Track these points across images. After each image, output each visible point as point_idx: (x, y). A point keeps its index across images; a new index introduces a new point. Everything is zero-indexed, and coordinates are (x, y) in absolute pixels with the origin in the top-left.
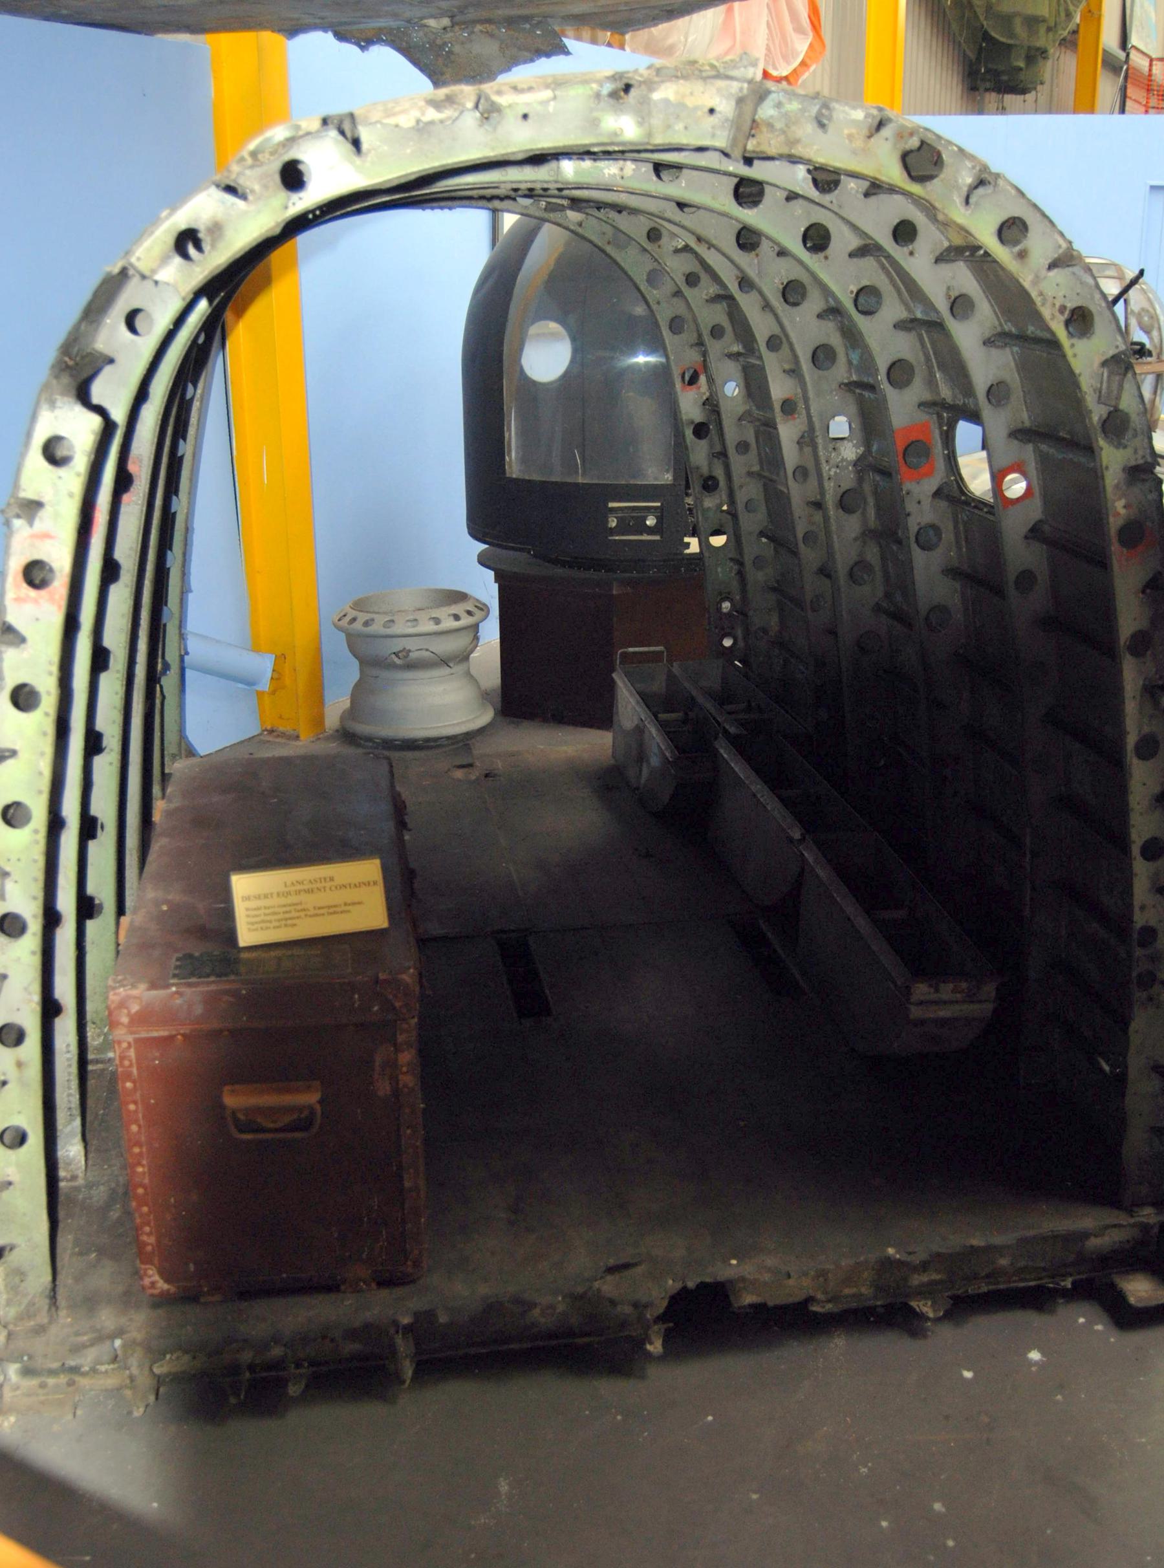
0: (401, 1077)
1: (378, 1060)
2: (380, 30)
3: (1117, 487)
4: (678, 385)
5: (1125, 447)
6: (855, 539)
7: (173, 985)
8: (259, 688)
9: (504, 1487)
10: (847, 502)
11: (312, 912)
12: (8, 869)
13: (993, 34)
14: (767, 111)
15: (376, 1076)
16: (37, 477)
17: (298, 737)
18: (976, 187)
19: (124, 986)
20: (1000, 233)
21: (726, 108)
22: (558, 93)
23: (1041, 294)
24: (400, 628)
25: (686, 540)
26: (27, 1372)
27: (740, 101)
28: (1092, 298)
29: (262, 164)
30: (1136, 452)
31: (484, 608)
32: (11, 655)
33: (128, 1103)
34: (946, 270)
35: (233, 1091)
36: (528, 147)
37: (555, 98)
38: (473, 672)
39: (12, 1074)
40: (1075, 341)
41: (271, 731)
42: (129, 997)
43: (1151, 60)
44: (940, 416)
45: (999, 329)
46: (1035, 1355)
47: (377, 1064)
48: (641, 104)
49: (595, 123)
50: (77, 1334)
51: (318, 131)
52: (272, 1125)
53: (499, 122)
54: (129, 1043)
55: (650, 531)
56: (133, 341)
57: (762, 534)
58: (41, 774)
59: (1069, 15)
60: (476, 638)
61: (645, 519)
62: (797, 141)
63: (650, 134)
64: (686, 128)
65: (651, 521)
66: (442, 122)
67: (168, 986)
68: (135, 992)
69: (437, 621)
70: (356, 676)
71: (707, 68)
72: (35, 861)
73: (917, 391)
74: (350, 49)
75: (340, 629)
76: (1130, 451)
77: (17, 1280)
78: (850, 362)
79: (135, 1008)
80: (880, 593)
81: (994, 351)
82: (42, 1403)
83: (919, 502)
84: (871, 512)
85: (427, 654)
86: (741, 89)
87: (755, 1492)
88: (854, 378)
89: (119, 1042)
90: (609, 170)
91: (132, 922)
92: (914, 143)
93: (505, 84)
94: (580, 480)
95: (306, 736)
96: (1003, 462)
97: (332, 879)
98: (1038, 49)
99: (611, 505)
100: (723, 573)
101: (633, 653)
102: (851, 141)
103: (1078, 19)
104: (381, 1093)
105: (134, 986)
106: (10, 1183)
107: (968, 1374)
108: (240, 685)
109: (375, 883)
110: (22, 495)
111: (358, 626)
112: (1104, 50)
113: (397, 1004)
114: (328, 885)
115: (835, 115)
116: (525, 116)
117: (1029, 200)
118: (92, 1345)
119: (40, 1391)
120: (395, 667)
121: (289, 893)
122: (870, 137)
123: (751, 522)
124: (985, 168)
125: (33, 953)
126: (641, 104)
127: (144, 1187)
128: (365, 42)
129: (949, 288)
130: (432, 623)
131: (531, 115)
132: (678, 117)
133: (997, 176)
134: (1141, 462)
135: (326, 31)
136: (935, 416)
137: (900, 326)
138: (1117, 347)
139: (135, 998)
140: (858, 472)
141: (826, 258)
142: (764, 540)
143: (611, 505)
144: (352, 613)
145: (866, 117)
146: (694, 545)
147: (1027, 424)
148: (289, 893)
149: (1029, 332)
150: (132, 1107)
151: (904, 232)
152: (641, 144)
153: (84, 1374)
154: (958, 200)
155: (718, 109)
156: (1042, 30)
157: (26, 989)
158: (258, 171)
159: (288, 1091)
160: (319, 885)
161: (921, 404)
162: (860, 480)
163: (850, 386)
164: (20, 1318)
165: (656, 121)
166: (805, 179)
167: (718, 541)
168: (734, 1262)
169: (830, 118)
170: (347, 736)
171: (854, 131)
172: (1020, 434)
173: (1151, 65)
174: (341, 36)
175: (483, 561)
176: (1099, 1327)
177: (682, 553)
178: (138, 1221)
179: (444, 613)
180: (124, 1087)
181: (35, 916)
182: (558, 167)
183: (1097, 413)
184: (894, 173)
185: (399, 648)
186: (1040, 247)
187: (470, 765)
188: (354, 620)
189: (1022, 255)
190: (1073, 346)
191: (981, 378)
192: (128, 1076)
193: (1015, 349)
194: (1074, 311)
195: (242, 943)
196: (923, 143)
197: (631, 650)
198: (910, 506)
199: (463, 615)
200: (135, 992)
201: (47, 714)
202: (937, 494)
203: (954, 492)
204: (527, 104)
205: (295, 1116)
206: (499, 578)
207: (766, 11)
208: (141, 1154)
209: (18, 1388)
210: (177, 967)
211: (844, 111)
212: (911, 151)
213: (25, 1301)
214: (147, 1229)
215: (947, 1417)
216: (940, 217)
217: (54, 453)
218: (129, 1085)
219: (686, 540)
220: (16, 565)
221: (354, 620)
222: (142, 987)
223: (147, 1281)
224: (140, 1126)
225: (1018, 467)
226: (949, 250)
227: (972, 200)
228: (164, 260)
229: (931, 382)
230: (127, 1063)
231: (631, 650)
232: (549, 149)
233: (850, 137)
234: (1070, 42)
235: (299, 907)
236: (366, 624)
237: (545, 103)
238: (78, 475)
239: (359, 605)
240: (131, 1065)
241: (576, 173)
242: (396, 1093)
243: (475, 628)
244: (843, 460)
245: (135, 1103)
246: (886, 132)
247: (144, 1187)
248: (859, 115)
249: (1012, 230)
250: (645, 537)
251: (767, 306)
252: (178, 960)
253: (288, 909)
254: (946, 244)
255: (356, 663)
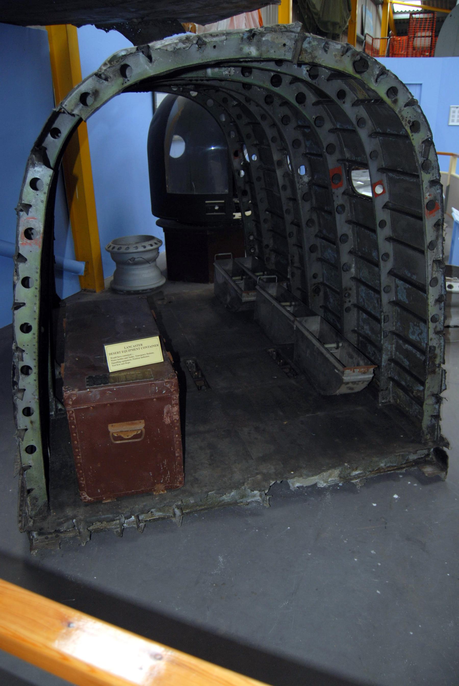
0: (174, 416)
1: (165, 411)
2: (114, 24)
3: (426, 188)
4: (232, 157)
5: (429, 173)
6: (308, 211)
7: (88, 388)
8: (80, 274)
9: (221, 559)
10: (305, 197)
11: (135, 357)
12: (24, 349)
13: (321, 29)
14: (306, 45)
15: (165, 417)
16: (29, 196)
17: (95, 292)
18: (381, 75)
19: (69, 390)
20: (387, 93)
21: (290, 44)
22: (228, 37)
23: (402, 116)
24: (132, 250)
25: (234, 214)
26: (40, 534)
27: (296, 41)
28: (420, 117)
29: (113, 66)
30: (433, 175)
31: (160, 241)
32: (21, 266)
33: (73, 433)
34: (356, 109)
35: (112, 426)
36: (215, 59)
37: (227, 39)
38: (158, 265)
39: (29, 426)
40: (413, 134)
41: (85, 290)
42: (72, 394)
43: (373, 39)
44: (345, 164)
45: (374, 131)
46: (396, 496)
47: (165, 412)
48: (258, 42)
49: (241, 49)
50: (59, 519)
51: (135, 53)
52: (127, 437)
53: (205, 49)
54: (72, 411)
55: (217, 211)
56: (53, 141)
57: (267, 210)
58: (35, 312)
59: (345, 22)
60: (158, 253)
61: (214, 207)
62: (316, 57)
63: (261, 54)
64: (275, 52)
65: (217, 208)
66: (184, 48)
67: (86, 389)
68: (74, 392)
69: (145, 247)
70: (115, 268)
71: (283, 28)
72: (34, 345)
73: (337, 155)
74: (102, 32)
75: (108, 251)
76: (431, 174)
77: (35, 501)
78: (306, 146)
79: (74, 398)
80: (317, 231)
81: (373, 140)
82: (47, 544)
83: (337, 196)
84: (314, 201)
85: (141, 259)
86: (295, 36)
87: (309, 553)
88: (307, 151)
89: (69, 411)
90: (225, 72)
91: (66, 365)
92: (358, 58)
93: (207, 34)
94: (195, 193)
95: (98, 291)
96: (375, 181)
97: (142, 345)
98: (337, 34)
99: (207, 202)
100: (251, 226)
101: (222, 256)
102: (335, 57)
103: (348, 24)
104: (167, 423)
105: (73, 390)
106: (30, 466)
107: (375, 505)
108: (73, 274)
109: (157, 345)
110: (23, 202)
111: (115, 250)
112: (357, 36)
113: (172, 390)
114: (140, 347)
115: (330, 47)
116: (215, 47)
117: (399, 81)
118: (65, 522)
119: (46, 540)
120: (129, 264)
121: (126, 351)
122: (342, 56)
123: (263, 206)
124: (384, 68)
125: (35, 380)
126: (258, 42)
127: (81, 464)
128: (107, 28)
129: (357, 116)
130: (143, 248)
131: (217, 46)
132: (272, 47)
133: (388, 71)
134: (435, 179)
135: (92, 25)
136: (343, 165)
137: (331, 131)
138: (428, 136)
139: (74, 394)
140: (310, 186)
141: (304, 106)
142: (267, 213)
143: (207, 202)
144: (113, 245)
145: (341, 47)
146: (238, 215)
147: (384, 166)
148: (126, 351)
149: (387, 132)
150: (75, 435)
151: (341, 94)
152: (259, 58)
153: (62, 532)
154: (373, 80)
155: (287, 44)
156: (338, 28)
157: (33, 394)
158: (112, 69)
159: (133, 424)
160: (137, 347)
161: (338, 160)
162: (310, 188)
163: (305, 155)
164: (36, 515)
165: (264, 48)
166: (306, 74)
167: (248, 213)
168: (292, 473)
169: (328, 48)
170: (113, 290)
171: (337, 53)
172: (382, 170)
173: (373, 41)
174: (98, 27)
175: (158, 224)
176: (416, 485)
177: (232, 219)
178: (78, 476)
179: (147, 244)
180: (71, 427)
181: (35, 366)
182: (206, 72)
183: (421, 160)
184: (350, 70)
185: (130, 258)
186: (402, 99)
187: (163, 299)
188: (114, 248)
189: (395, 102)
190: (412, 136)
191: (368, 148)
192: (73, 424)
193: (381, 138)
194: (413, 122)
195: (110, 371)
196: (361, 57)
197: (220, 254)
198: (335, 198)
199: (154, 244)
200: (74, 392)
201: (36, 288)
202: (344, 193)
203: (351, 193)
204: (216, 42)
205: (135, 433)
206: (164, 231)
207: (245, 19)
208: (79, 452)
209: (37, 540)
210: (87, 382)
211: (333, 45)
212: (357, 61)
213: (38, 509)
214: (82, 479)
215: (370, 520)
216: (366, 87)
217: (34, 184)
218: (73, 427)
219: (234, 214)
220: (22, 229)
221: (114, 248)
222: (76, 390)
223: (83, 497)
224: (78, 442)
225: (380, 183)
226: (358, 101)
227: (379, 80)
228: (77, 105)
229: (342, 152)
230: (72, 419)
231: (220, 254)
232: (223, 60)
233: (335, 56)
234: (345, 33)
235: (130, 356)
236: (119, 249)
237: (222, 41)
238: (45, 193)
239: (115, 242)
240: (74, 419)
241: (212, 74)
242: (172, 422)
243: (158, 249)
244: (304, 182)
245: (76, 433)
246: (349, 53)
247: (81, 464)
248: (339, 47)
249: (392, 91)
250: (215, 214)
251: (274, 125)
252: (87, 378)
253: (126, 357)
254: (356, 99)
255: (114, 264)
